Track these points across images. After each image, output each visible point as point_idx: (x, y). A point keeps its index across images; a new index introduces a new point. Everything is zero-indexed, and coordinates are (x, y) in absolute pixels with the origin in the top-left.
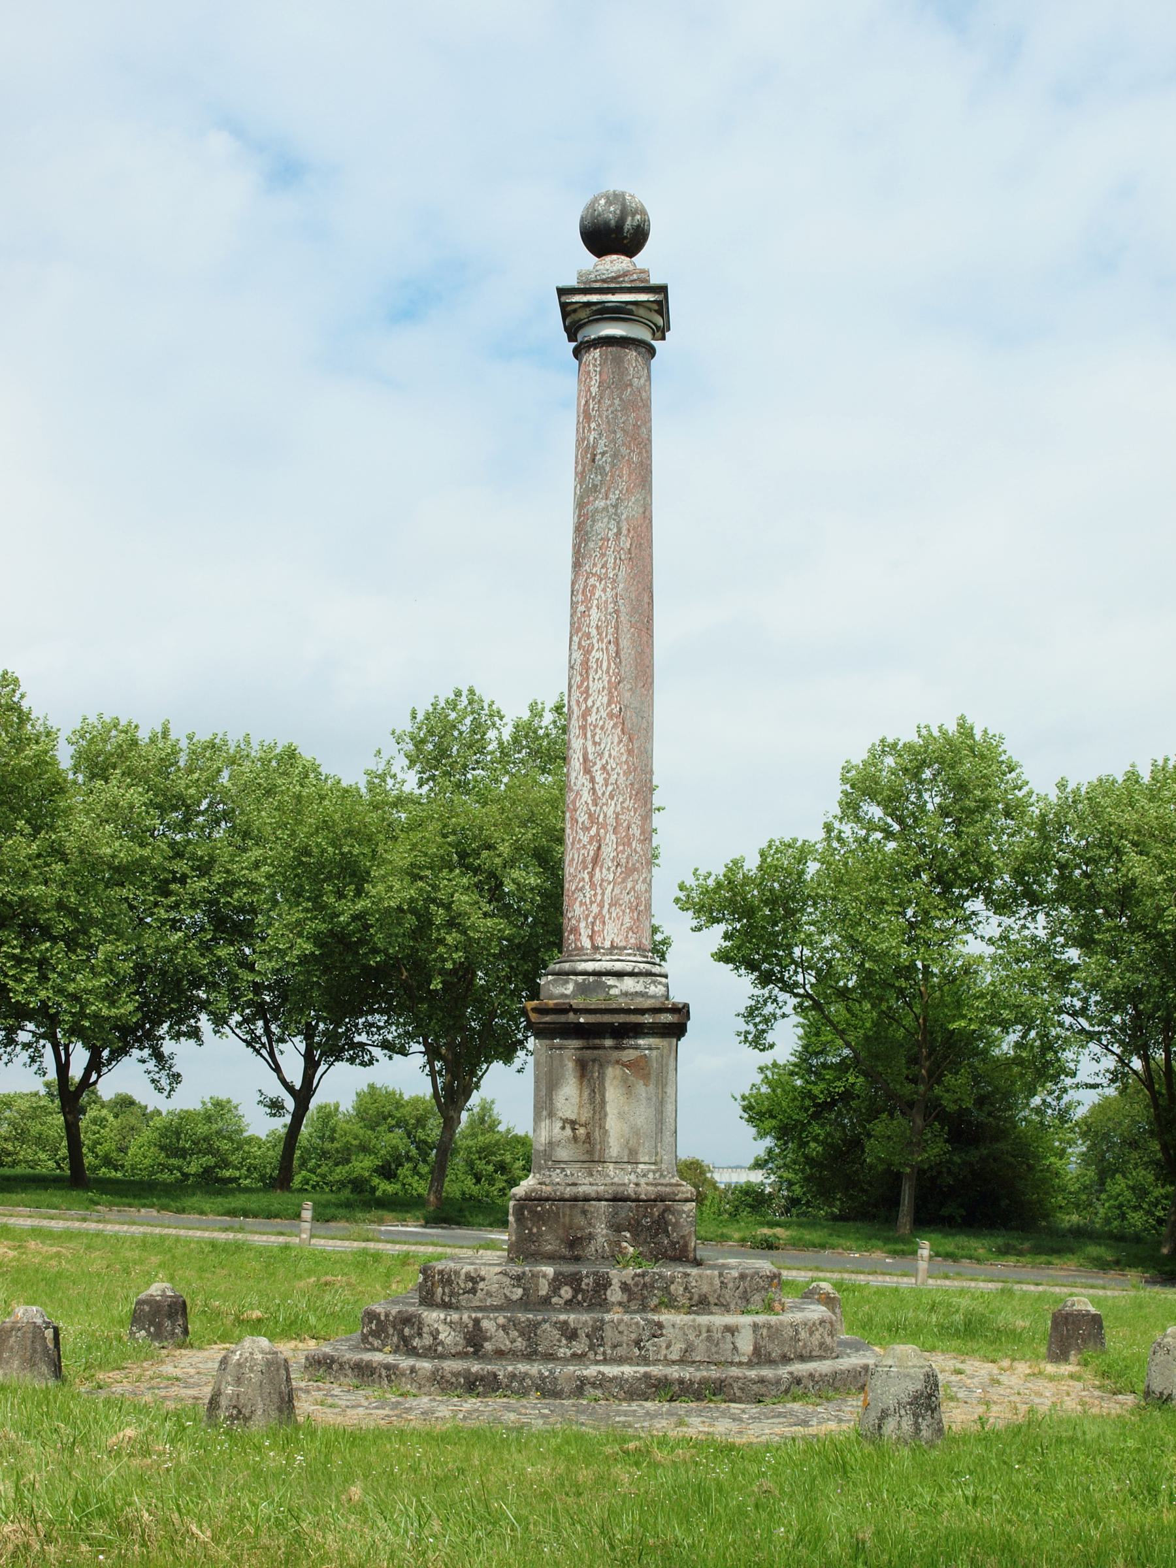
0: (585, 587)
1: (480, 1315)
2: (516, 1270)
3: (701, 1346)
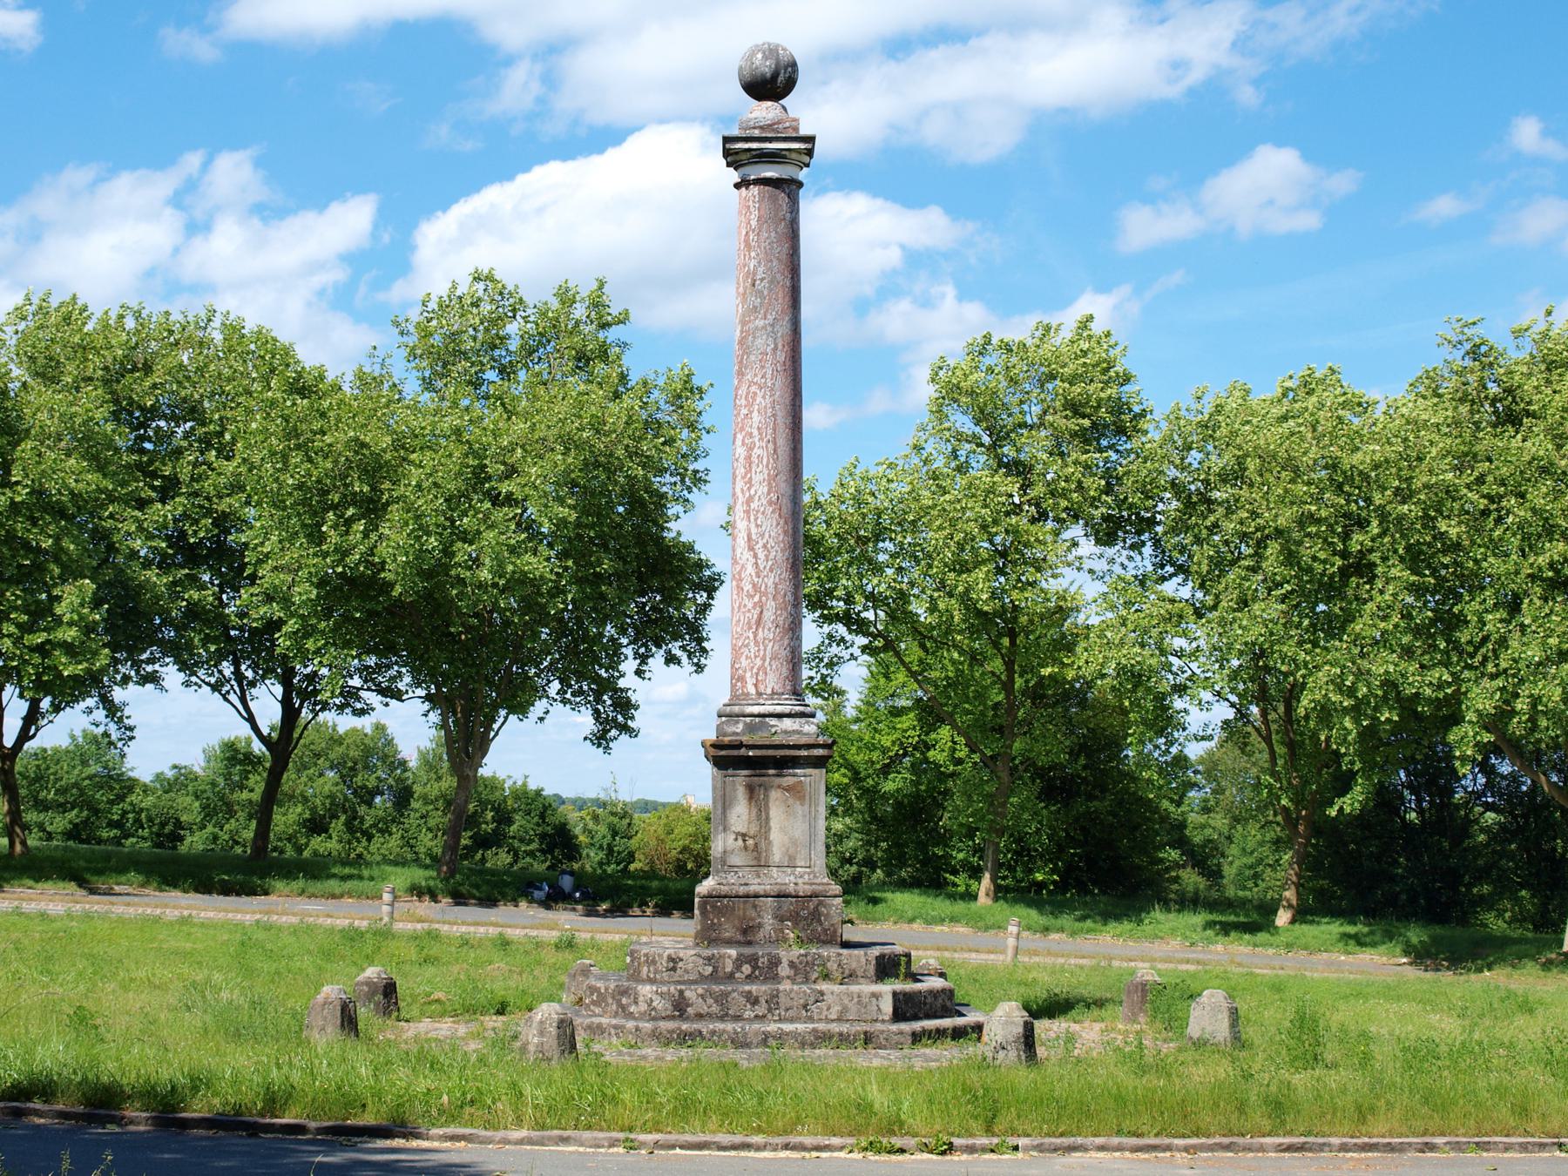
3: (853, 1007)
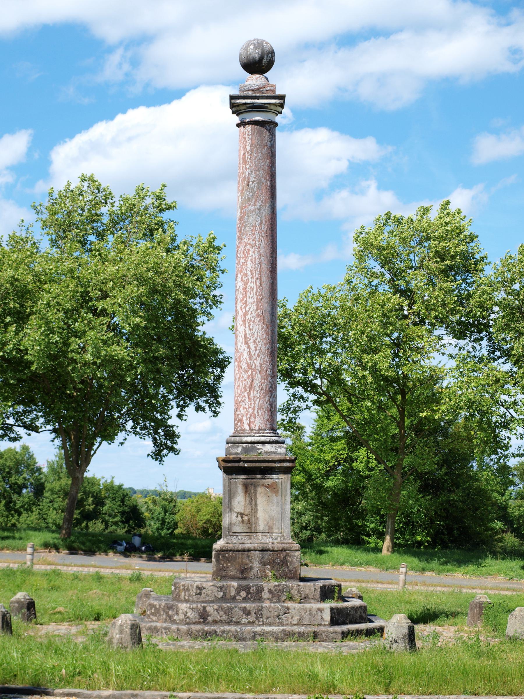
0: (245, 250)
1: (206, 605)
2: (220, 584)
